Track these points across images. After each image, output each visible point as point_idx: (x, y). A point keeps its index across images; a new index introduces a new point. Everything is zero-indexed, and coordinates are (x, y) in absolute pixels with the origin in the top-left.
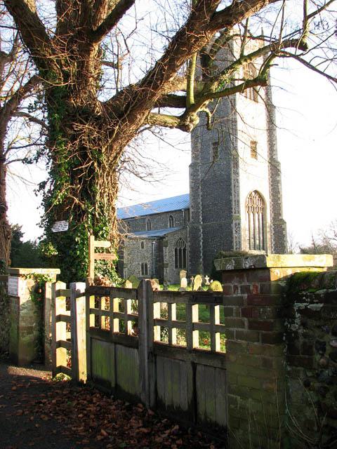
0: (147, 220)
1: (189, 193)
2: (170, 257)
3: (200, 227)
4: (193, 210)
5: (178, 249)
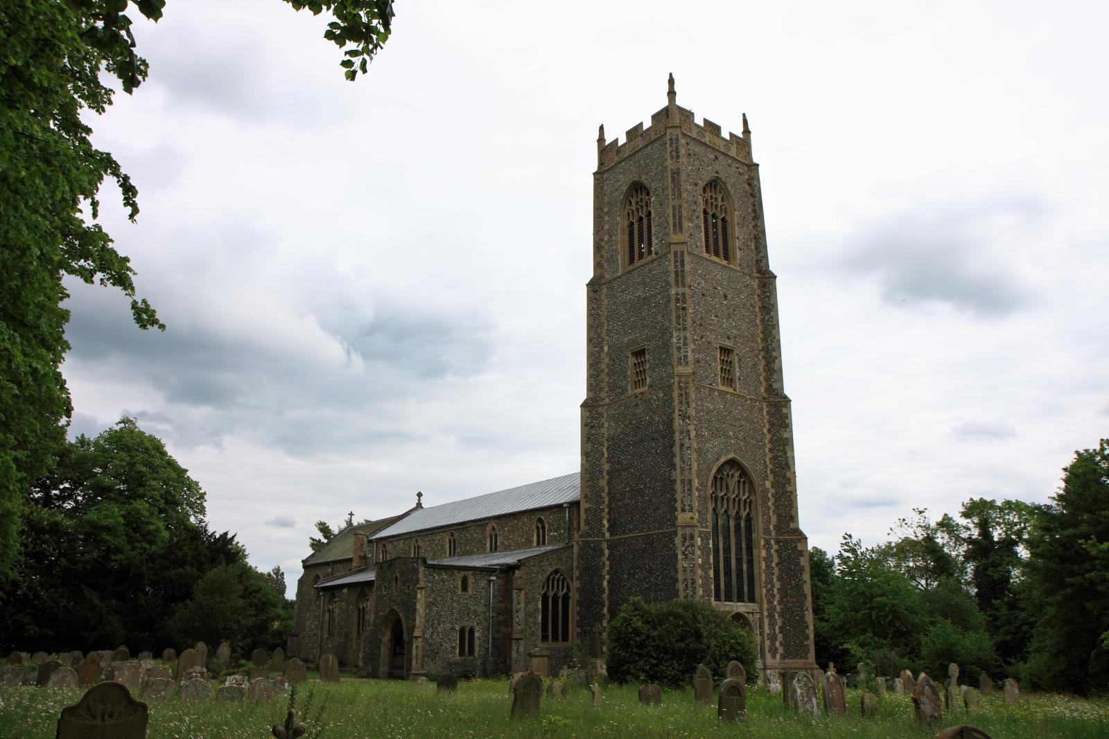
0: (488, 529)
1: (580, 471)
2: (529, 615)
3: (604, 545)
4: (588, 506)
5: (551, 594)
